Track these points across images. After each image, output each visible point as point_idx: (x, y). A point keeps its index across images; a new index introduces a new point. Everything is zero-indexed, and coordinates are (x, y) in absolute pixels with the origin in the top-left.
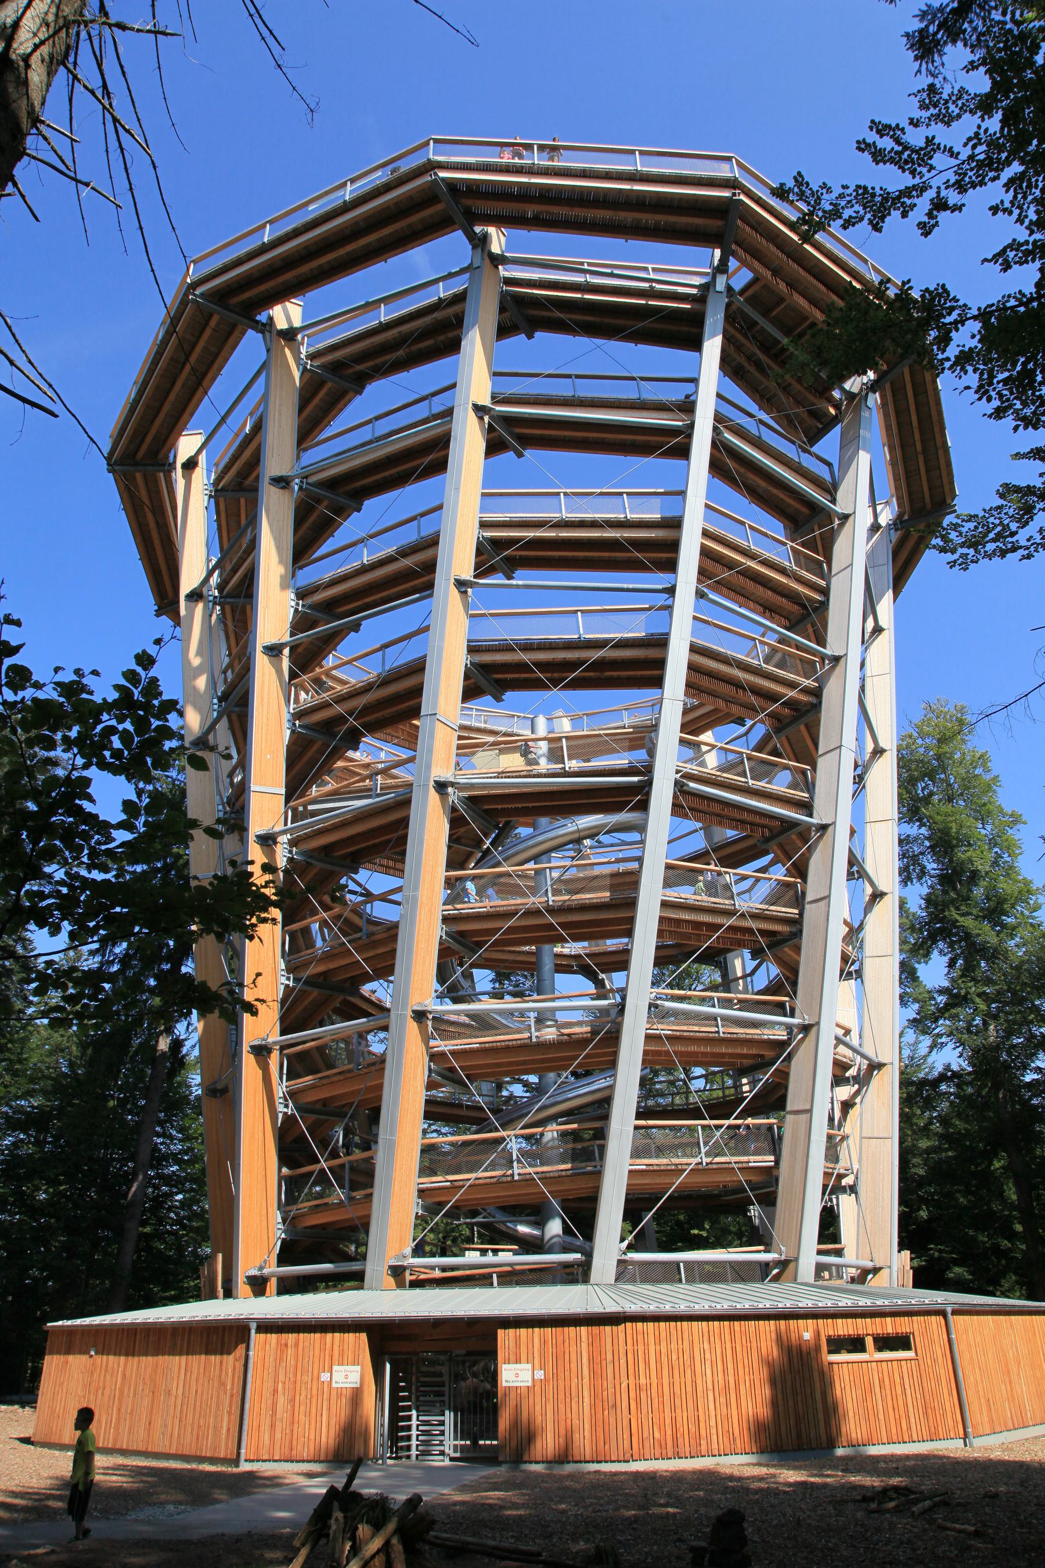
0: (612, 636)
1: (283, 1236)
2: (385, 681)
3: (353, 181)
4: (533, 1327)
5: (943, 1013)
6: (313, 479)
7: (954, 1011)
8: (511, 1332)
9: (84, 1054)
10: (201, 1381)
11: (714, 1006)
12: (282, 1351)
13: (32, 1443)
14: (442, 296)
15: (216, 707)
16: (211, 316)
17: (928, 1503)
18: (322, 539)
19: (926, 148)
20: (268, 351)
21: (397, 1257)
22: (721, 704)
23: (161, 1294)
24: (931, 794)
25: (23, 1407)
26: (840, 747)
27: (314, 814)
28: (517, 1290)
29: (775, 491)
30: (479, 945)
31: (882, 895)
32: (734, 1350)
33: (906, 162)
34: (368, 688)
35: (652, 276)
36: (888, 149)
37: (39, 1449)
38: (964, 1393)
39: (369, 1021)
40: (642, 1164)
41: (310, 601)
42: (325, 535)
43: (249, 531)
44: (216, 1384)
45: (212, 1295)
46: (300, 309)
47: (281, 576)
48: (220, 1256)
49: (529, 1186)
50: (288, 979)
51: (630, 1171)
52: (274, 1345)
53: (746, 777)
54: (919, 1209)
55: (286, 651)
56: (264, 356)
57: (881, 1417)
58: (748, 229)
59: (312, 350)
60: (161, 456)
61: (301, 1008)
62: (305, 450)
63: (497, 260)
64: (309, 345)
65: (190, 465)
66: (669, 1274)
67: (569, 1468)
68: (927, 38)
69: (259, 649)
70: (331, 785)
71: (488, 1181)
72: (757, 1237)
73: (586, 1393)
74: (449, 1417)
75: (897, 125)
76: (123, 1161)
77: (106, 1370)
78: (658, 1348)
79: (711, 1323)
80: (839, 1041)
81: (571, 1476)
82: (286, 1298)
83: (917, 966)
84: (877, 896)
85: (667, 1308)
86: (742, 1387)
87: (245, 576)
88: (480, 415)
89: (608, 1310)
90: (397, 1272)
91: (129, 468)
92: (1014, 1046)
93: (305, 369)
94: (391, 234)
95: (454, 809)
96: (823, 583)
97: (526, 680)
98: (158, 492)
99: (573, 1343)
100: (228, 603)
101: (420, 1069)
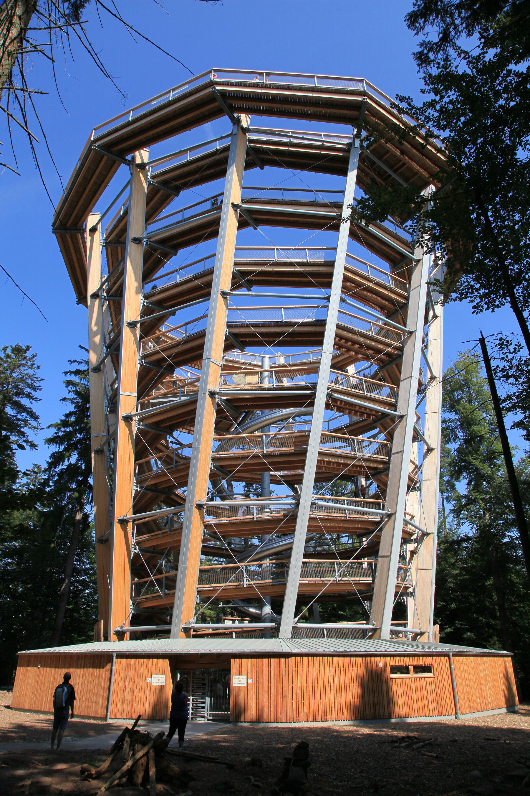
0: (298, 320)
1: (133, 612)
2: (187, 341)
3: (174, 90)
4: (248, 658)
5: (463, 508)
6: (153, 239)
7: (469, 507)
8: (238, 660)
9: (39, 520)
10: (90, 680)
11: (344, 504)
12: (128, 667)
13: (11, 708)
14: (218, 148)
15: (105, 351)
16: (102, 157)
17: (421, 744)
18: (158, 269)
19: (423, 107)
20: (131, 174)
21: (186, 623)
22: (353, 354)
23: (79, 638)
24: (462, 398)
25: (9, 692)
26: (411, 376)
27: (154, 405)
28: (243, 640)
29: (384, 247)
30: (230, 472)
31: (432, 449)
32: (345, 671)
33: (414, 114)
34: (178, 344)
35: (323, 139)
36: (405, 108)
37: (14, 711)
38: (456, 694)
39: (175, 509)
40: (306, 580)
41: (150, 300)
42: (159, 267)
43: (122, 264)
44: (97, 682)
45: (99, 640)
46: (148, 153)
47: (136, 288)
48: (102, 621)
49: (251, 590)
50: (137, 487)
51: (300, 584)
52: (124, 664)
53: (364, 391)
54: (451, 604)
55: (139, 325)
56: (129, 177)
57: (415, 705)
58: (371, 116)
59: (153, 174)
60: (79, 225)
61: (144, 501)
62: (149, 224)
63: (245, 131)
64: (152, 172)
65: (93, 230)
66: (318, 634)
67: (261, 725)
68: (423, 55)
69: (125, 324)
70: (163, 391)
71: (232, 587)
72: (365, 617)
73: (272, 690)
74: (207, 700)
75: (409, 97)
76: (59, 573)
77: (46, 675)
78: (307, 669)
79: (334, 658)
80: (406, 523)
81: (263, 729)
82: (133, 642)
83: (455, 483)
84: (430, 450)
85: (313, 650)
86: (348, 689)
87: (120, 286)
88: (235, 209)
89: (284, 651)
90: (186, 630)
91: (63, 231)
92: (498, 524)
93: (150, 184)
94: (192, 117)
95: (218, 405)
96: (406, 294)
97: (256, 342)
98: (78, 243)
99: (267, 666)
100: (111, 300)
101: (199, 532)
